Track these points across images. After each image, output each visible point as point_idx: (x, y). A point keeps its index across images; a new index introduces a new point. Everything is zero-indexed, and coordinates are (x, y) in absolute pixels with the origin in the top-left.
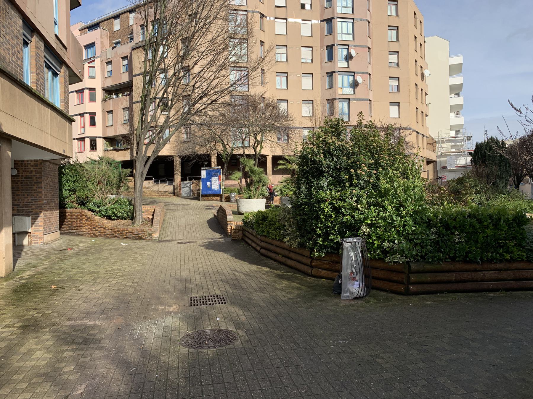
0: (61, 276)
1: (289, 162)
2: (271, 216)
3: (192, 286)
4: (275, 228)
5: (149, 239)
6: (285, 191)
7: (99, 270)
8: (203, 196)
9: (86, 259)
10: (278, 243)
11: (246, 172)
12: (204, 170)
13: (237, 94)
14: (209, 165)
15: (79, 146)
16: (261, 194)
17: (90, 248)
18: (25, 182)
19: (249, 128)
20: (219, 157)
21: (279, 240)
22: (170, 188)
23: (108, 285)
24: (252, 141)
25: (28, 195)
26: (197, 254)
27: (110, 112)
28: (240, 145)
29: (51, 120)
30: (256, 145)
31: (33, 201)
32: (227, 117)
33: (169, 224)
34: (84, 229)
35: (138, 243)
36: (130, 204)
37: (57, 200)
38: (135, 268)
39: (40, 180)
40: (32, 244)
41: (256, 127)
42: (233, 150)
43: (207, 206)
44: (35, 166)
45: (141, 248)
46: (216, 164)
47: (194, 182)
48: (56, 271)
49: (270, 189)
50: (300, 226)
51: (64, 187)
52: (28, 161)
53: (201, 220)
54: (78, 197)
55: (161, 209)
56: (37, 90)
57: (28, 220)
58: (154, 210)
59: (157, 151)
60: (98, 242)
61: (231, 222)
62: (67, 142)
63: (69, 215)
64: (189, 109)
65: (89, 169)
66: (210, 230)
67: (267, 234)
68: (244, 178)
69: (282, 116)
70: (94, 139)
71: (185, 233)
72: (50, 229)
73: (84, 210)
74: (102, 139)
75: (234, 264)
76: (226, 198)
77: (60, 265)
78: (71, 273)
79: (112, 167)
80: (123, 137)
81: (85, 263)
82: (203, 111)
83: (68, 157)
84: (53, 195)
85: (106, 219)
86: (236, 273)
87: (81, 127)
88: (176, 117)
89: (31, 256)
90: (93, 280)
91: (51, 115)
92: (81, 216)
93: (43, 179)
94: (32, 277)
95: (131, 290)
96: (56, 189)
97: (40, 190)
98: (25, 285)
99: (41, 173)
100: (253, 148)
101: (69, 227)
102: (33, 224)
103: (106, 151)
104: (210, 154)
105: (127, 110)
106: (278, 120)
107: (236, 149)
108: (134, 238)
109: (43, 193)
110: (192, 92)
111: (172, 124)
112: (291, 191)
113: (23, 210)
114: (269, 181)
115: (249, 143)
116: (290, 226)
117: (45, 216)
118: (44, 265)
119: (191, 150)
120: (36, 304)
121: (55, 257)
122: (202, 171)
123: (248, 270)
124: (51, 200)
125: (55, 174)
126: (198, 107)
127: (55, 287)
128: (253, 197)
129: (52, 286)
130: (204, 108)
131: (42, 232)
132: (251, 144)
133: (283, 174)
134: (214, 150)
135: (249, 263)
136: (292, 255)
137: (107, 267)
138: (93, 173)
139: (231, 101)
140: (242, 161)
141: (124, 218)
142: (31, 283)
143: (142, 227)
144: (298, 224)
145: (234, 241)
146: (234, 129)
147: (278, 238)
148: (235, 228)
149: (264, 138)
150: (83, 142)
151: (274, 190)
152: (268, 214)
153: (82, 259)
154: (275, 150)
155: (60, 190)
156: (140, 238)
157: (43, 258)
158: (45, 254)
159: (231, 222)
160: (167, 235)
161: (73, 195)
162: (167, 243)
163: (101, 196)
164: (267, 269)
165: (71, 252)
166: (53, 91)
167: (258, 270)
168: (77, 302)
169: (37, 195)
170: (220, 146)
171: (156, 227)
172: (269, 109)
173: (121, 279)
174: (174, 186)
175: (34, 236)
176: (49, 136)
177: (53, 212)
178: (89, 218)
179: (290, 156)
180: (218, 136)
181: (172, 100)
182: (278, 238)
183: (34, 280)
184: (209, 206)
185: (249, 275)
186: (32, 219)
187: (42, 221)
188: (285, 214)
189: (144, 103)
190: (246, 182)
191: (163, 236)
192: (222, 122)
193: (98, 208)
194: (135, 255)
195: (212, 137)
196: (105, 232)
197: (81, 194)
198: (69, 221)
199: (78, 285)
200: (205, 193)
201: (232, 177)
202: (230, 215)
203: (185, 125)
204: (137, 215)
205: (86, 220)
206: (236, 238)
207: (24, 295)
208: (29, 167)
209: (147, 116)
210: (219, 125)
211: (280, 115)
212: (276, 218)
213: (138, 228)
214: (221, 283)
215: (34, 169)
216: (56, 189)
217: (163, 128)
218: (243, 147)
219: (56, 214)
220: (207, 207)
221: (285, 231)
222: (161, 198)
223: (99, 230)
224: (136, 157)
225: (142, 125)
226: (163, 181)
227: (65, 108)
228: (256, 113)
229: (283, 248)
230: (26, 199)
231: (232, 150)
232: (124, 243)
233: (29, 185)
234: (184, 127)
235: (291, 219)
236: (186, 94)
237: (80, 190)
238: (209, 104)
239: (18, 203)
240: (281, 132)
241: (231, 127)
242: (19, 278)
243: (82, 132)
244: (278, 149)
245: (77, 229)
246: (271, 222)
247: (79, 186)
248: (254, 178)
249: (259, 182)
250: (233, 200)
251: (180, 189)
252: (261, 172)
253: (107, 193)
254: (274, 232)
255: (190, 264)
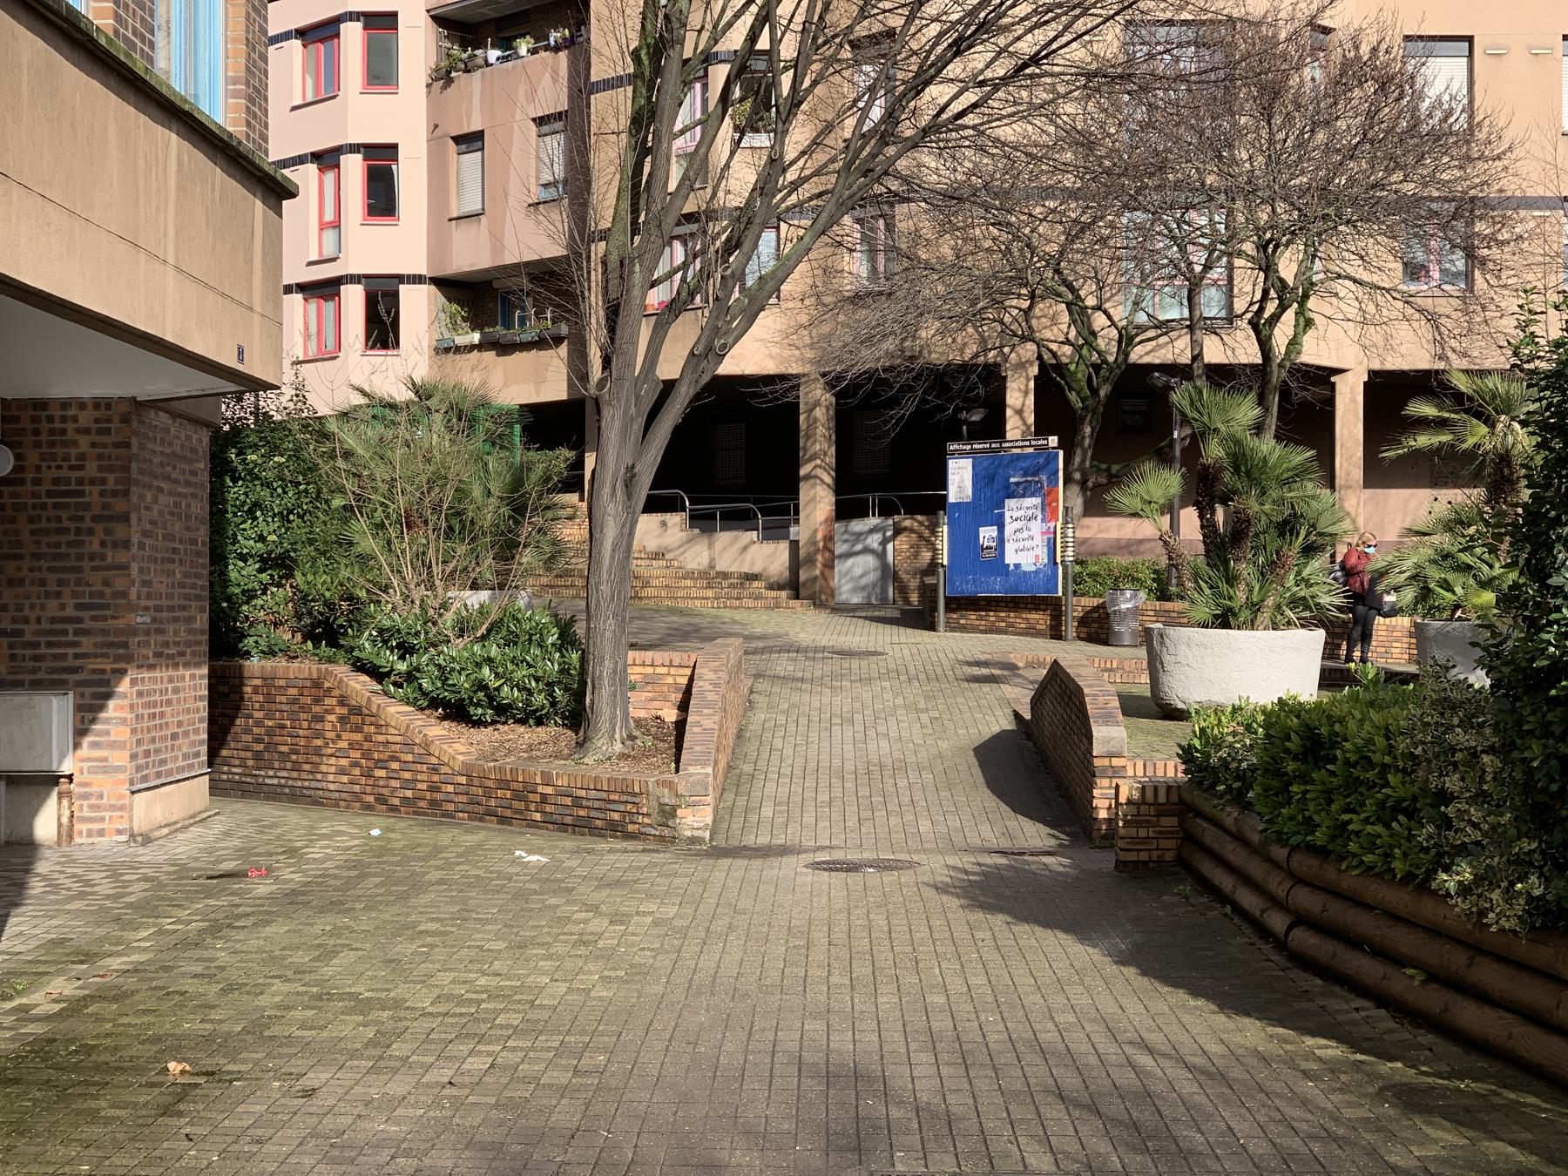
0: (213, 1015)
1: (1479, 409)
2: (1357, 732)
3: (895, 1113)
4: (1382, 805)
5: (662, 839)
6: (1448, 587)
7: (401, 991)
8: (958, 604)
9: (336, 932)
10: (1399, 899)
11: (1206, 468)
12: (961, 454)
13: (1169, 15)
14: (994, 427)
15: (313, 329)
16: (1295, 602)
17: (358, 868)
18: (52, 512)
19: (1230, 213)
20: (1050, 382)
21: (1409, 877)
22: (770, 557)
23: (446, 1074)
24: (1248, 285)
25: (60, 583)
26: (922, 933)
27: (471, 141)
28: (1174, 312)
29: (180, 188)
30: (1271, 308)
31: (86, 615)
32: (1101, 152)
33: (765, 755)
34: (329, 766)
35: (602, 853)
36: (567, 638)
37: (202, 610)
38: (587, 991)
39: (119, 505)
40: (77, 840)
41: (1271, 202)
42: (1131, 339)
43: (978, 664)
44: (100, 432)
45: (618, 883)
46: (1031, 419)
47: (907, 523)
48: (189, 985)
49: (1349, 572)
50: (1542, 798)
51: (235, 541)
52: (65, 404)
53: (944, 745)
54: (305, 598)
55: (724, 675)
56: (116, 32)
57: (59, 709)
58: (691, 679)
59: (710, 349)
60: (398, 840)
61: (1116, 762)
62: (257, 308)
63: (256, 690)
64: (891, 117)
65: (360, 451)
66: (991, 801)
67: (1333, 838)
68: (1197, 504)
69: (1437, 136)
70: (387, 286)
71: (852, 809)
72: (163, 762)
73: (331, 667)
74: (424, 287)
75: (1133, 1007)
76: (1083, 621)
77: (206, 954)
78: (263, 1001)
79: (478, 443)
80: (533, 278)
81: (334, 953)
82: (970, 120)
83: (259, 385)
84: (182, 585)
85: (443, 718)
86: (1145, 1060)
87: (323, 226)
88: (821, 157)
89: (71, 899)
90: (371, 1043)
91: (180, 164)
92: (317, 701)
93: (134, 499)
94: (74, 1008)
95: (566, 1114)
96: (198, 554)
97: (121, 557)
98: (42, 1048)
99: (127, 469)
100: (1254, 324)
101: (258, 756)
102: (81, 732)
103: (447, 350)
104: (997, 365)
105: (559, 125)
106: (1411, 159)
107: (1151, 333)
108: (583, 827)
109: (134, 568)
110: (910, 19)
111: (793, 199)
112: (1485, 585)
113: (36, 658)
114: (1346, 525)
115: (1230, 296)
116: (1480, 797)
117: (140, 694)
118: (129, 949)
119: (890, 345)
120: (92, 1151)
121: (183, 914)
122: (952, 464)
123: (1214, 1048)
124: (171, 609)
125: (193, 473)
126: (942, 101)
127: (183, 1072)
128: (1245, 615)
129: (172, 1065)
130: (975, 106)
131: (124, 776)
132: (1240, 305)
133: (1434, 484)
134: (1024, 339)
135: (1222, 1007)
136: (1489, 975)
137: (445, 978)
138: (381, 472)
139: (1131, 61)
140: (1185, 403)
141: (535, 718)
142: (72, 1041)
143: (625, 769)
144: (1528, 787)
145: (1133, 871)
146: (1139, 216)
147: (1399, 866)
148: (1136, 795)
149: (1318, 265)
150: (329, 306)
151: (1382, 574)
152: (1341, 721)
153: (317, 930)
154: (1387, 338)
155: (218, 559)
156: (616, 830)
157: (128, 915)
158: (138, 891)
159: (1116, 762)
160: (754, 818)
161: (279, 585)
162: (757, 863)
163: (417, 594)
164: (1331, 1050)
165: (264, 888)
166: (191, 37)
167: (1272, 1048)
168: (293, 1160)
169: (106, 583)
170: (1054, 320)
171: (698, 770)
172: (1357, 93)
173: (514, 1049)
174: (794, 545)
175: (86, 796)
176: (171, 271)
177: (181, 671)
178: (356, 711)
179: (1483, 373)
180: (1047, 258)
181: (798, 65)
182: (1399, 866)
183: (84, 1028)
184: (985, 664)
185: (1222, 1077)
186: (79, 708)
187: (124, 721)
188: (1450, 728)
189: (650, 89)
190: (1208, 527)
191: (737, 825)
192: (1069, 181)
193: (402, 658)
194: (585, 922)
195: (1013, 266)
196: (438, 790)
197: (316, 580)
198: (259, 724)
199: (296, 1065)
200: (967, 588)
201: (1126, 498)
202: (1108, 719)
203: (863, 202)
204: (602, 700)
205: (342, 719)
206: (1144, 856)
207: (35, 1100)
208: (70, 435)
209: (662, 161)
210: (1054, 198)
211: (1424, 129)
212: (1390, 750)
213: (605, 772)
214: (1054, 1112)
215: (93, 445)
216: (198, 554)
217: (746, 224)
218: (1193, 325)
219: (194, 682)
220: (977, 671)
221: (1449, 827)
222: (727, 614)
223: (407, 775)
224: (601, 384)
225: (635, 212)
226: (738, 519)
227: (248, 124)
228: (1278, 120)
229: (1435, 932)
230: (53, 604)
231: (1126, 339)
232: (529, 852)
233: (66, 531)
234: (858, 213)
235: (1486, 759)
236: (877, 28)
237: (314, 560)
238: (1005, 80)
239: (14, 620)
240: (1430, 229)
241: (1125, 206)
242: (13, 1009)
243: (328, 252)
244: (1403, 332)
245: (297, 767)
246: (1356, 772)
247: (311, 542)
248: (1253, 505)
249: (1287, 527)
250: (1124, 629)
251: (829, 565)
252: (1299, 474)
253: (449, 578)
254: (1379, 829)
255: (882, 989)
